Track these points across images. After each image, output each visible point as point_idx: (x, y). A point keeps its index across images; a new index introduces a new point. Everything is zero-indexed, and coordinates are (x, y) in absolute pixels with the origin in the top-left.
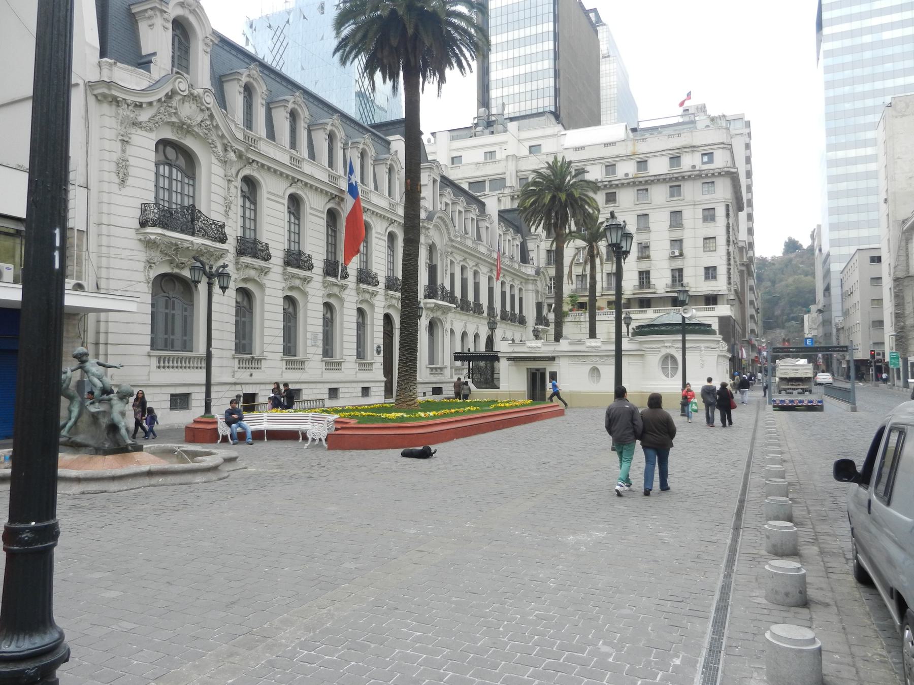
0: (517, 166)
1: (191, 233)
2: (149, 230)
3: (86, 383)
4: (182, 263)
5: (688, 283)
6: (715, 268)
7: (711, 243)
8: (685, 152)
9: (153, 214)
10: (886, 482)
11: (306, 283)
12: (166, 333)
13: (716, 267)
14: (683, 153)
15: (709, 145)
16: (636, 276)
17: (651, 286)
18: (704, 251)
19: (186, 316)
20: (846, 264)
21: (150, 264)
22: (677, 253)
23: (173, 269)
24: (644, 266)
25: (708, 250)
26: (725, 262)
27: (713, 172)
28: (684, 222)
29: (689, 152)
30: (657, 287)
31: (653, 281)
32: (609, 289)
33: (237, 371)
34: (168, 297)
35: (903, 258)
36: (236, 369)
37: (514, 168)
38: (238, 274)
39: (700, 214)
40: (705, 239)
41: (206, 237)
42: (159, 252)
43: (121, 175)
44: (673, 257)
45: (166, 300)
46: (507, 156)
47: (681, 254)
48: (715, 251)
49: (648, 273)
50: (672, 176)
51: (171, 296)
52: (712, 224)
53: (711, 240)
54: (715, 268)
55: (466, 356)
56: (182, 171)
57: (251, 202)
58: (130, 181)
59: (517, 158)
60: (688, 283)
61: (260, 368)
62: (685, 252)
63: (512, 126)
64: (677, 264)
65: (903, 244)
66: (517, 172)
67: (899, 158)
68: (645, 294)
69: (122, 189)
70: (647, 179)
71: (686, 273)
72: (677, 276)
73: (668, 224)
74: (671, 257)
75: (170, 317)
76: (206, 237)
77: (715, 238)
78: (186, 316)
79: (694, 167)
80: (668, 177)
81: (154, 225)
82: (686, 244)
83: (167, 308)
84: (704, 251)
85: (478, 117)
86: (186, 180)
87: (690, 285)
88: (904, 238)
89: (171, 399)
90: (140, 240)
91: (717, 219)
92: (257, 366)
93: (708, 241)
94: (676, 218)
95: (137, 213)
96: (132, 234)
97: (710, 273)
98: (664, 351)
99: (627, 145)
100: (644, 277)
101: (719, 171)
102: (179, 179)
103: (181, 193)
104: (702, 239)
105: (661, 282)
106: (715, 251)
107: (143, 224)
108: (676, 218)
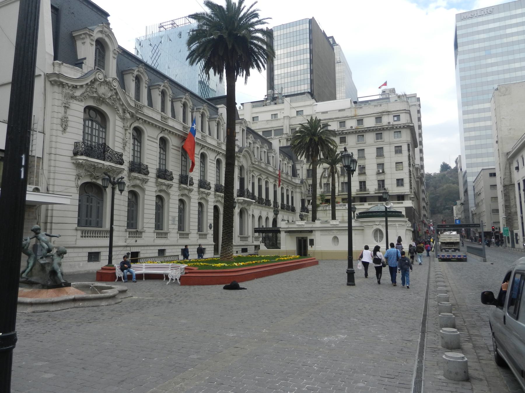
1: (103, 159)
6: (402, 180)
7: (400, 166)
8: (384, 115)
9: (81, 149)
13: (403, 179)
14: (383, 115)
15: (397, 111)
16: (358, 184)
18: (396, 170)
19: (98, 207)
20: (476, 177)
21: (78, 177)
22: (381, 171)
24: (362, 178)
25: (398, 169)
26: (408, 176)
27: (400, 126)
28: (385, 154)
29: (386, 115)
30: (370, 190)
31: (368, 187)
32: (343, 191)
33: (128, 239)
34: (88, 196)
36: (127, 237)
39: (393, 149)
40: (396, 163)
44: (378, 173)
47: (383, 172)
48: (402, 170)
49: (365, 182)
50: (377, 128)
51: (90, 195)
53: (400, 164)
54: (402, 180)
60: (387, 188)
62: (385, 170)
64: (381, 177)
65: (508, 166)
67: (503, 118)
68: (363, 194)
70: (363, 129)
72: (381, 183)
73: (375, 154)
74: (377, 173)
76: (112, 161)
80: (375, 128)
82: (386, 166)
83: (88, 202)
84: (396, 170)
87: (389, 189)
88: (508, 163)
90: (73, 163)
94: (380, 152)
95: (72, 148)
96: (69, 159)
97: (400, 182)
98: (375, 227)
100: (363, 184)
101: (403, 125)
105: (372, 187)
106: (402, 170)
107: (75, 154)
108: (380, 152)
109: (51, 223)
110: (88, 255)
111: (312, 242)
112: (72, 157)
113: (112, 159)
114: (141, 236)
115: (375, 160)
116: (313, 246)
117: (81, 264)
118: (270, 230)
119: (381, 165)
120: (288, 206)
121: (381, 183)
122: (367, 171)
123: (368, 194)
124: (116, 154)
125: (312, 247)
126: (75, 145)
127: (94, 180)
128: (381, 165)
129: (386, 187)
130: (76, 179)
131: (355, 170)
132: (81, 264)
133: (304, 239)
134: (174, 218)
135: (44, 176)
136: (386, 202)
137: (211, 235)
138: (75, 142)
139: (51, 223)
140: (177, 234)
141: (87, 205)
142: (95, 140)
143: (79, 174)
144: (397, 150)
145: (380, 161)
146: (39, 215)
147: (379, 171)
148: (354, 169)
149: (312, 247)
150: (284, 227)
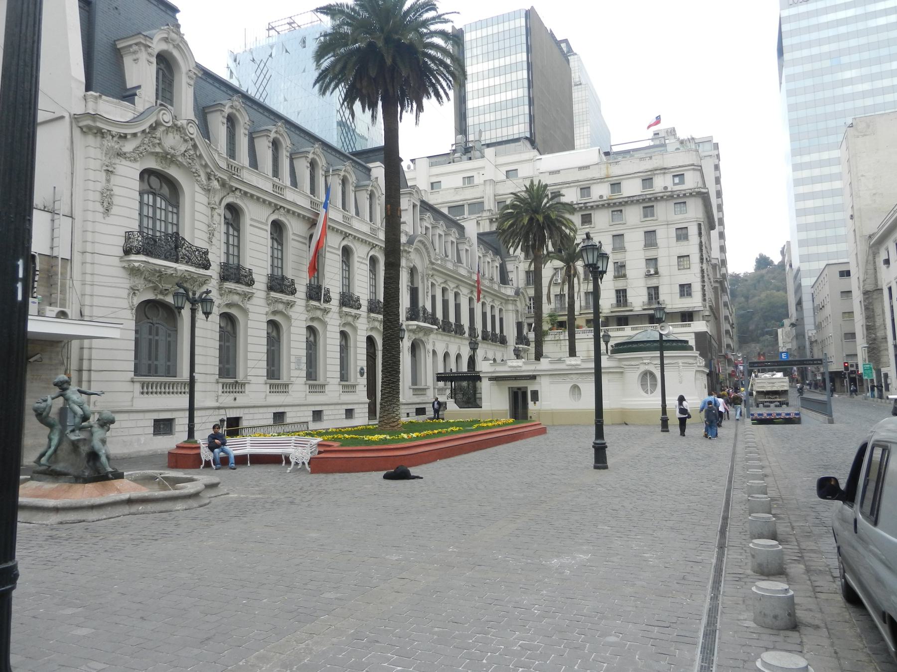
4: (166, 290)
9: (136, 243)
17: (628, 304)
21: (134, 291)
22: (652, 272)
23: (156, 295)
26: (699, 279)
28: (658, 241)
30: (634, 305)
31: (630, 299)
34: (152, 323)
39: (673, 233)
40: (679, 257)
44: (648, 276)
47: (657, 273)
48: (689, 268)
51: (154, 322)
52: (685, 243)
53: (685, 259)
57: (234, 229)
59: (494, 183)
62: (660, 270)
63: (489, 151)
64: (653, 282)
66: (495, 196)
72: (654, 293)
73: (643, 243)
76: (190, 263)
86: (170, 209)
90: (124, 268)
94: (650, 238)
95: (122, 242)
102: (163, 207)
105: (638, 300)
106: (689, 268)
107: (127, 252)
108: (650, 238)
111: (535, 396)
112: (121, 257)
113: (189, 259)
116: (537, 402)
118: (468, 376)
119: (652, 261)
121: (654, 293)
125: (535, 403)
128: (652, 261)
138: (126, 232)
145: (651, 254)
147: (649, 271)
149: (535, 403)
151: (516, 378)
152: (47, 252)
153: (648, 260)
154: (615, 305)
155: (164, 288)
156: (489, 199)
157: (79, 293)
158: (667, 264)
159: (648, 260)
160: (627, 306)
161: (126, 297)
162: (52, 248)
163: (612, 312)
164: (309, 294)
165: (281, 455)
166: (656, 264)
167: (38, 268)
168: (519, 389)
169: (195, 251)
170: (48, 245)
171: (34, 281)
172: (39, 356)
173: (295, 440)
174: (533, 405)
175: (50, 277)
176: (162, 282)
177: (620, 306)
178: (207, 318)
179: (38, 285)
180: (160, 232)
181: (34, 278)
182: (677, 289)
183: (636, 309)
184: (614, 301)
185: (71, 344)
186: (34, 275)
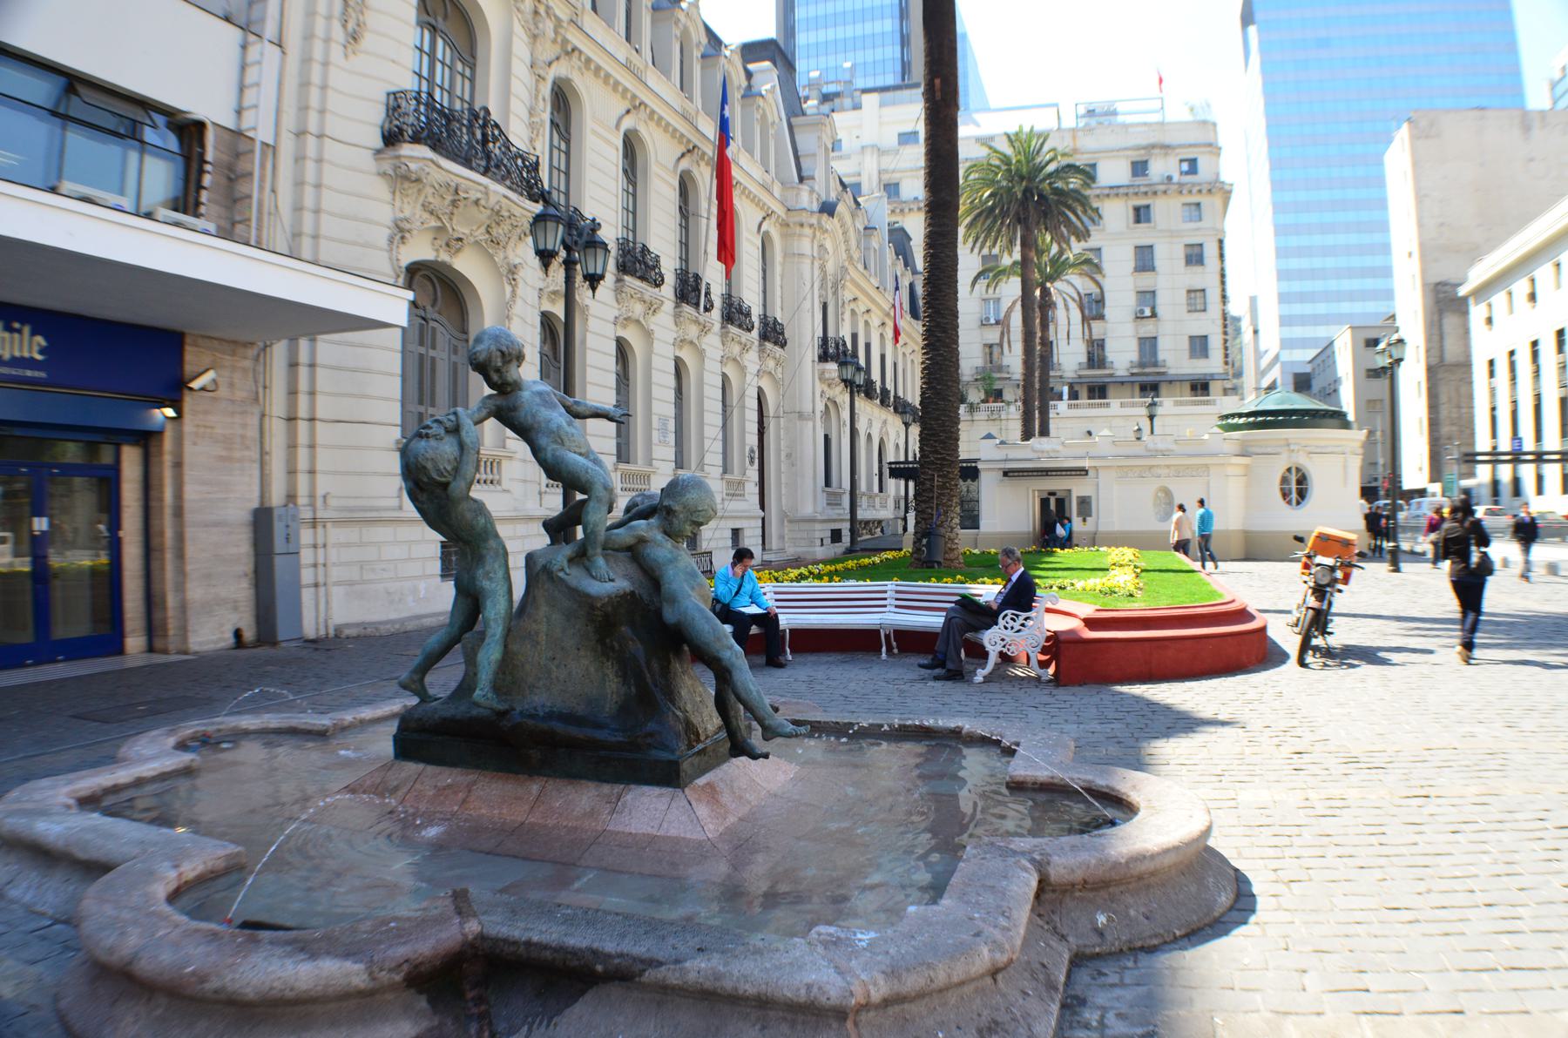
0: (879, 163)
1: (482, 169)
2: (407, 150)
3: (276, 513)
4: (460, 239)
5: (1164, 361)
9: (412, 118)
10: (513, 574)
11: (651, 312)
12: (421, 402)
13: (1206, 337)
15: (1191, 146)
17: (1107, 365)
19: (455, 364)
20: (1319, 350)
21: (401, 232)
22: (1148, 312)
23: (437, 250)
26: (1220, 329)
28: (1157, 263)
30: (1116, 365)
31: (1111, 355)
33: (546, 492)
34: (424, 319)
35: (1436, 338)
36: (544, 488)
37: (875, 166)
38: (544, 280)
39: (1180, 253)
40: (1189, 291)
41: (508, 183)
42: (419, 207)
43: (351, 26)
44: (1139, 317)
45: (421, 325)
46: (863, 148)
47: (1154, 315)
48: (1204, 310)
51: (429, 316)
52: (1198, 269)
53: (1198, 294)
55: (967, 467)
56: (453, 47)
57: (561, 137)
58: (368, 41)
59: (881, 152)
60: (1164, 361)
61: (499, 483)
62: (1159, 310)
63: (870, 100)
64: (1148, 329)
66: (880, 173)
69: (352, 57)
71: (1163, 344)
72: (1148, 345)
73: (1132, 264)
75: (428, 365)
76: (508, 183)
77: (1203, 290)
78: (455, 364)
79: (1169, 178)
81: (416, 139)
82: (1161, 300)
83: (421, 343)
85: (809, 85)
86: (459, 67)
87: (1169, 364)
89: (442, 553)
90: (384, 175)
91: (1206, 261)
92: (490, 477)
93: (1193, 295)
94: (1145, 259)
95: (378, 115)
96: (366, 161)
99: (1063, 137)
102: (448, 61)
103: (449, 93)
104: (1184, 292)
105: (1122, 356)
106: (1204, 310)
107: (391, 138)
108: (1145, 259)
109: (312, 419)
110: (439, 555)
111: (1085, 505)
112: (378, 152)
113: (508, 172)
114: (497, 477)
115: (1131, 279)
116: (1088, 519)
117: (422, 585)
118: (900, 468)
119: (1147, 297)
120: (885, 392)
121: (1148, 345)
122: (1107, 312)
123: (1111, 375)
124: (521, 157)
125: (1084, 520)
126: (387, 105)
127: (444, 257)
128: (1147, 297)
129: (1161, 356)
130: (391, 241)
131: (602, 277)
132: (422, 585)
133: (1059, 495)
134: (664, 420)
135: (278, 222)
136: (974, 396)
137: (753, 484)
138: (388, 94)
139: (312, 419)
140: (720, 482)
141: (421, 356)
142: (463, 94)
143: (401, 220)
144: (1191, 256)
145: (1146, 281)
146: (265, 387)
147: (1142, 311)
148: (599, 271)
149: (1084, 520)
150: (989, 458)
151: (1045, 472)
152: (228, 121)
153: (1141, 293)
154: (1085, 366)
155: (456, 235)
156: (870, 178)
157: (288, 229)
158: (1170, 301)
159: (1141, 293)
160: (1105, 368)
161: (386, 247)
162: (239, 112)
163: (1133, 374)
164: (681, 290)
165: (877, 632)
166: (1204, 297)
167: (209, 156)
168: (1052, 494)
169: (517, 157)
170: (232, 102)
171: (200, 187)
172: (210, 375)
173: (897, 592)
174: (1082, 523)
175: (234, 176)
176: (454, 221)
177: (1093, 368)
178: (594, 289)
179: (209, 200)
180: (462, 100)
181: (199, 181)
182: (1185, 344)
183: (1119, 373)
184: (1084, 359)
185: (271, 353)
186: (201, 172)
